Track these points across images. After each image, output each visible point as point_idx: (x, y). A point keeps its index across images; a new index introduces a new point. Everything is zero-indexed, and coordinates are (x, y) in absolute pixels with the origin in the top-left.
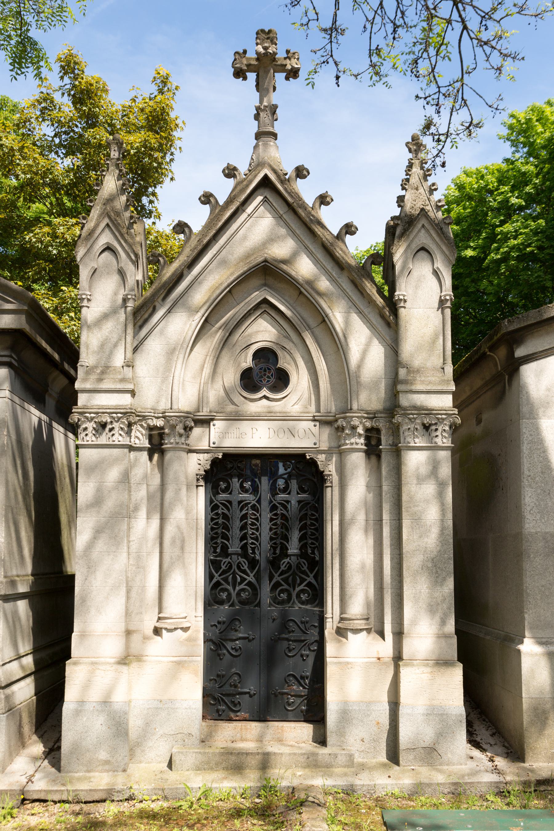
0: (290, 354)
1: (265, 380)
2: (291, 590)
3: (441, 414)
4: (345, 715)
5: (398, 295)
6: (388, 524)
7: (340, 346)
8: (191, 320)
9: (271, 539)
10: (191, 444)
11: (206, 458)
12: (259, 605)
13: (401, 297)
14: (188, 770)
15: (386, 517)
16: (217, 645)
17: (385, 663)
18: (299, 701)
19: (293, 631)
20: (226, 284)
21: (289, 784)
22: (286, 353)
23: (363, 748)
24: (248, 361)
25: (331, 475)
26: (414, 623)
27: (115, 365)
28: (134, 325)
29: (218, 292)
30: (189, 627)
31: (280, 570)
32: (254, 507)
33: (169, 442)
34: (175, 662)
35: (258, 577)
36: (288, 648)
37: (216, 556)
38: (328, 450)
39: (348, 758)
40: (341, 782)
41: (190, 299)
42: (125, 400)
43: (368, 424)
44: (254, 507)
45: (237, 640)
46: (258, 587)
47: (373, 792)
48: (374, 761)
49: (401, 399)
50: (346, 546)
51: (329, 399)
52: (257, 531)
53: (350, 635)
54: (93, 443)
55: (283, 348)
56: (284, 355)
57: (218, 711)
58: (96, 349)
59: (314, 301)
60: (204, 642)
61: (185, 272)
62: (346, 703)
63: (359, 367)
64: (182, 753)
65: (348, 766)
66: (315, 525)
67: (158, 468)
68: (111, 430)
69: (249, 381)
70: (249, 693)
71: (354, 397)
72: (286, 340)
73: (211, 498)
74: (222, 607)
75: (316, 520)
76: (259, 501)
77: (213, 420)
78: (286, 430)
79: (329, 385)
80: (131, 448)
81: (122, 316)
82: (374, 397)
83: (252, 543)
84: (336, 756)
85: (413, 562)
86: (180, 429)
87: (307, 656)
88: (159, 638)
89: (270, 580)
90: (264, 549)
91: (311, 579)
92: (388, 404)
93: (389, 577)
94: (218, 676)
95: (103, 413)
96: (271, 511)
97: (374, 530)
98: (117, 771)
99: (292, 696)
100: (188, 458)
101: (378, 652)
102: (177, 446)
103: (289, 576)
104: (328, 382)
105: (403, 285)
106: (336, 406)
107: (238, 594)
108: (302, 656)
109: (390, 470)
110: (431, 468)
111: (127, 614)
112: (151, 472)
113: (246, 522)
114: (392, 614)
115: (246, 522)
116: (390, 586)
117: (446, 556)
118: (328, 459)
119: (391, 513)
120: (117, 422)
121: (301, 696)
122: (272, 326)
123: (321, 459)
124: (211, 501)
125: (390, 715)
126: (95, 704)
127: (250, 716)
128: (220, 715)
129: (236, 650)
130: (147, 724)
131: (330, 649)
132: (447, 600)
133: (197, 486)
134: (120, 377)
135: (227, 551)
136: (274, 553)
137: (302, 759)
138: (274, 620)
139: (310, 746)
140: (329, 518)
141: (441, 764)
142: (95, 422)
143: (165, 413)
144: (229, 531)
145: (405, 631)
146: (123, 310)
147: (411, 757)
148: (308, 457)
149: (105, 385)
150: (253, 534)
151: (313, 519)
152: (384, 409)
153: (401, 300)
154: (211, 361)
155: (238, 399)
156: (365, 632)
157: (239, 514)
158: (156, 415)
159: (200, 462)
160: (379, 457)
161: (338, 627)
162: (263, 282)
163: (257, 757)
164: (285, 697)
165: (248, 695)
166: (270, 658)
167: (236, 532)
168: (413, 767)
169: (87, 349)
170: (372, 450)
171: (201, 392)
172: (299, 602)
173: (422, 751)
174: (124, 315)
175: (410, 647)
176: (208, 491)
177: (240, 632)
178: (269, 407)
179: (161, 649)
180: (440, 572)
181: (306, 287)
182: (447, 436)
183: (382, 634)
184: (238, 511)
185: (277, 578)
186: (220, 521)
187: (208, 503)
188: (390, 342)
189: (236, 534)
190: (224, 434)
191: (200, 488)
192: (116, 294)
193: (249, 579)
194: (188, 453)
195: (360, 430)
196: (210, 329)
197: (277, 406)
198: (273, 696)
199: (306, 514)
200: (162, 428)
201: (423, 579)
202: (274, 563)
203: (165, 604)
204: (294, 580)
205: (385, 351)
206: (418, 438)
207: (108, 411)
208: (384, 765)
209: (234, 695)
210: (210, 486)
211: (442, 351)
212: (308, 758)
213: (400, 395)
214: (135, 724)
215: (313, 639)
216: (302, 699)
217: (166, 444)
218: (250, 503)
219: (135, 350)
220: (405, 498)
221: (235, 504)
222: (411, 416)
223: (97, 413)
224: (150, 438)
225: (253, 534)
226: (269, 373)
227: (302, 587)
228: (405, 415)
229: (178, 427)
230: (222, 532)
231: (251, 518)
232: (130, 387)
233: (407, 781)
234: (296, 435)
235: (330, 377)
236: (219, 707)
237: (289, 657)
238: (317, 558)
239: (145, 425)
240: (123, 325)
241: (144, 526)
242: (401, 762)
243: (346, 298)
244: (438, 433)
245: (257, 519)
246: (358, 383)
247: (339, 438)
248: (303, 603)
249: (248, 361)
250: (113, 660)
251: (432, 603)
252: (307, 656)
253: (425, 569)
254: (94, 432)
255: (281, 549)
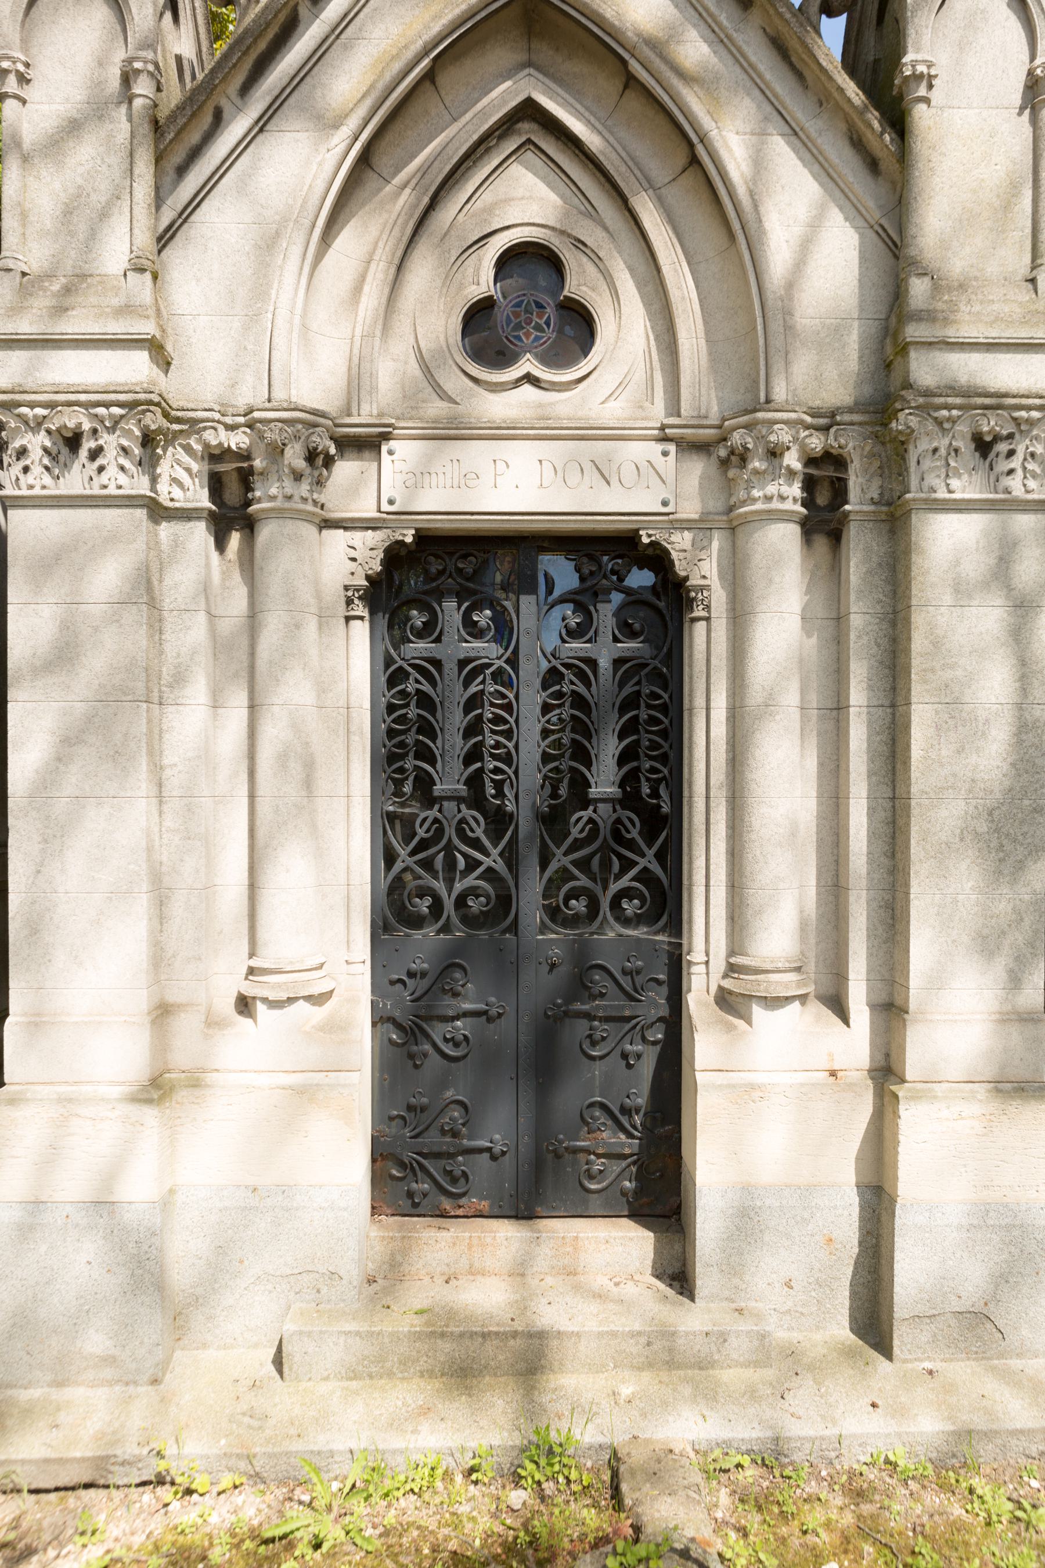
0: (596, 259)
1: (528, 335)
2: (598, 889)
3: (1029, 408)
4: (747, 1220)
5: (914, 64)
6: (864, 717)
7: (736, 226)
8: (323, 149)
9: (546, 758)
10: (329, 505)
11: (370, 543)
12: (514, 928)
13: (921, 68)
14: (326, 1379)
15: (858, 696)
16: (407, 1031)
17: (851, 1086)
18: (617, 1167)
19: (602, 995)
20: (419, 44)
21: (601, 1439)
22: (585, 259)
23: (790, 1304)
24: (481, 279)
25: (707, 587)
26: (937, 982)
27: (103, 270)
28: (159, 159)
29: (397, 66)
30: (332, 992)
31: (569, 840)
32: (498, 676)
33: (267, 494)
34: (291, 1088)
35: (511, 856)
36: (590, 1036)
37: (403, 805)
38: (701, 520)
39: (756, 1343)
40: (746, 1430)
41: (319, 92)
42: (133, 369)
43: (816, 443)
44: (498, 676)
45: (457, 1018)
46: (511, 883)
47: (833, 1454)
48: (818, 1337)
49: (913, 365)
50: (749, 776)
51: (704, 380)
52: (510, 739)
53: (757, 1011)
54: (45, 492)
55: (579, 244)
56: (580, 265)
57: (410, 1195)
58: (49, 224)
59: (666, 98)
60: (374, 1024)
61: (303, 12)
62: (747, 1190)
63: (790, 286)
64: (309, 1334)
65: (756, 1364)
66: (660, 722)
67: (242, 571)
68: (95, 454)
69: (486, 335)
70: (489, 1150)
71: (778, 365)
72: (587, 223)
73: (387, 651)
74: (417, 935)
75: (664, 709)
76: (513, 661)
77: (386, 437)
78: (588, 466)
79: (703, 342)
80: (158, 512)
81: (120, 126)
82: (830, 372)
83: (496, 770)
84: (723, 1337)
85: (940, 816)
86: (294, 456)
87: (639, 1056)
88: (249, 1021)
89: (544, 865)
90: (527, 789)
91: (647, 861)
92: (867, 390)
93: (864, 859)
94: (410, 1108)
95: (70, 404)
96: (545, 687)
97: (819, 734)
98: (135, 1383)
99: (599, 1156)
100: (321, 543)
101: (830, 1055)
102: (287, 505)
103: (593, 855)
104: (701, 333)
105: (927, 37)
106: (721, 401)
107: (461, 902)
108: (625, 1056)
109: (869, 572)
110: (992, 561)
111: (159, 960)
112: (223, 580)
113: (481, 715)
114: (870, 955)
115: (481, 715)
116: (864, 883)
117: (1026, 802)
118: (701, 546)
119: (870, 688)
120: (111, 430)
121: (625, 1157)
122: (548, 185)
123: (679, 545)
124: (389, 662)
125: (862, 1219)
126: (69, 1209)
127: (491, 1206)
128: (415, 1205)
129: (457, 1045)
130: (221, 1250)
131: (707, 1047)
132: (1027, 922)
133: (348, 619)
134: (115, 302)
135: (431, 791)
136: (554, 795)
137: (634, 1347)
138: (553, 966)
139: (647, 1293)
140: (700, 701)
141: (1001, 1356)
142: (49, 432)
143: (252, 412)
144: (434, 739)
145: (913, 1005)
146: (123, 109)
147: (924, 1337)
148: (645, 540)
149: (74, 325)
150: (655, 696)
151: (653, 709)
152: (856, 403)
153: (921, 76)
154: (380, 276)
155: (454, 382)
156: (797, 1003)
157: (459, 695)
158: (229, 420)
159: (353, 554)
160: (836, 537)
161: (721, 988)
162: (522, 57)
163: (512, 1342)
164: (582, 1157)
165: (486, 1156)
166: (544, 1061)
167: (452, 742)
168: (928, 1365)
169: (24, 226)
170: (823, 520)
171: (356, 360)
172: (617, 919)
173: (953, 1322)
174: (125, 126)
175: (921, 1049)
176: (378, 635)
177: (466, 998)
178: (540, 405)
179: (253, 1057)
180: (1008, 847)
181: (647, 52)
182: (1038, 471)
183: (838, 1006)
184: (459, 686)
185: (560, 860)
186: (413, 712)
187: (381, 666)
188: (875, 215)
189: (453, 746)
190: (418, 477)
191: (355, 624)
192: (101, 63)
193: (488, 862)
194: (321, 529)
195: (792, 460)
196: (380, 190)
197: (563, 405)
198: (550, 1156)
199: (638, 693)
200: (246, 456)
201: (963, 866)
202: (553, 820)
203: (262, 935)
204: (605, 865)
205: (862, 244)
206: (959, 476)
207: (83, 397)
208: (849, 1353)
209: (451, 1156)
210: (383, 621)
211: (1028, 230)
212: (649, 1344)
213: (913, 354)
214: (184, 1254)
215: (654, 1014)
216: (624, 1164)
217: (259, 501)
218: (488, 666)
219: (165, 238)
220: (918, 643)
221: (450, 668)
222: (945, 413)
223: (51, 405)
224: (216, 485)
225: (498, 745)
226: (540, 317)
227: (625, 882)
228: (926, 410)
229: (288, 452)
230: (417, 741)
231: (492, 705)
232: (147, 328)
233: (928, 1426)
234: (614, 481)
235: (706, 322)
236: (414, 1185)
237: (593, 1058)
238: (666, 809)
239: (198, 447)
240: (125, 153)
241: (199, 725)
242: (896, 1351)
243: (757, 92)
244: (1016, 463)
245: (508, 708)
246: (788, 328)
247: (729, 485)
248: (626, 922)
249: (483, 280)
250: (116, 1091)
251: (985, 932)
252: (639, 1056)
253: (969, 838)
254: (46, 461)
255: (572, 783)
